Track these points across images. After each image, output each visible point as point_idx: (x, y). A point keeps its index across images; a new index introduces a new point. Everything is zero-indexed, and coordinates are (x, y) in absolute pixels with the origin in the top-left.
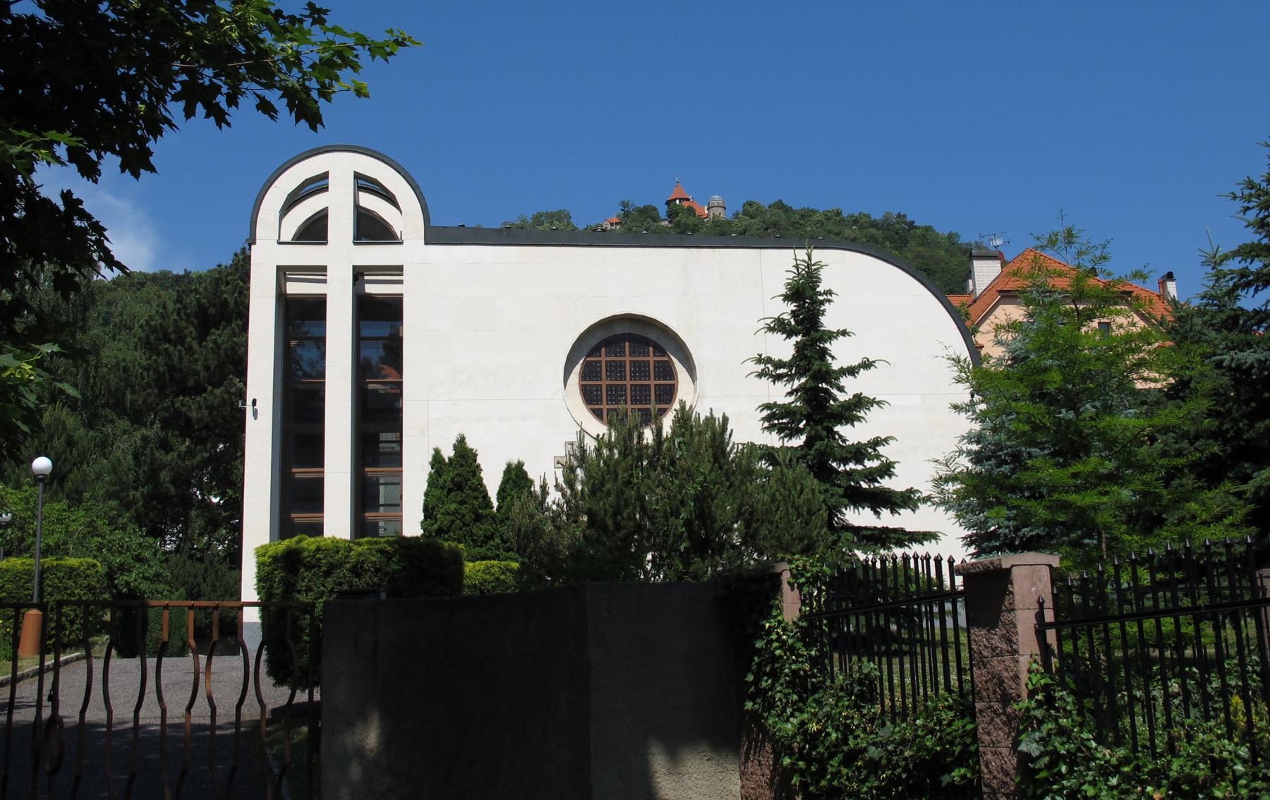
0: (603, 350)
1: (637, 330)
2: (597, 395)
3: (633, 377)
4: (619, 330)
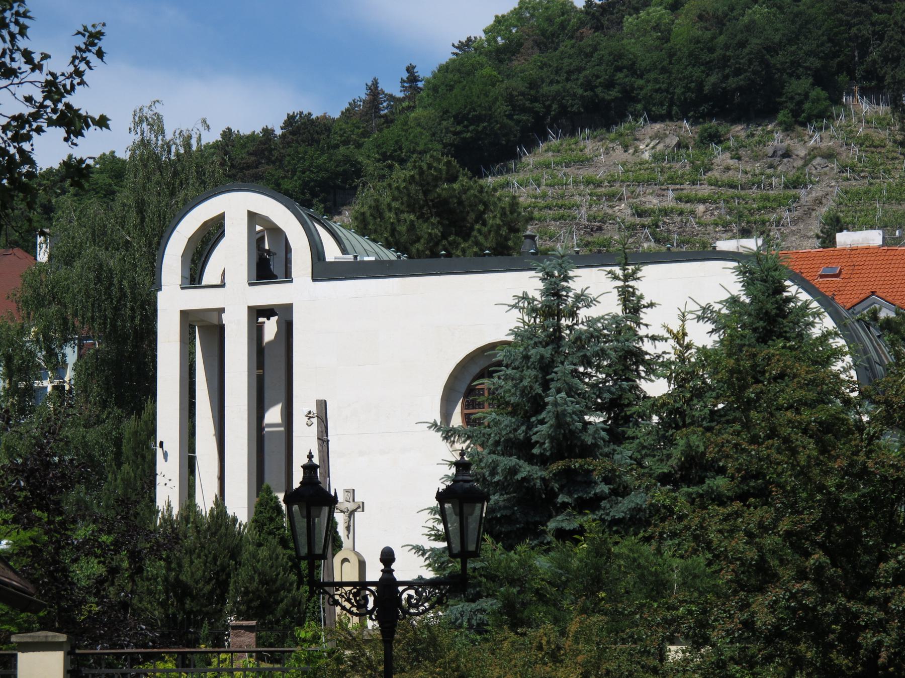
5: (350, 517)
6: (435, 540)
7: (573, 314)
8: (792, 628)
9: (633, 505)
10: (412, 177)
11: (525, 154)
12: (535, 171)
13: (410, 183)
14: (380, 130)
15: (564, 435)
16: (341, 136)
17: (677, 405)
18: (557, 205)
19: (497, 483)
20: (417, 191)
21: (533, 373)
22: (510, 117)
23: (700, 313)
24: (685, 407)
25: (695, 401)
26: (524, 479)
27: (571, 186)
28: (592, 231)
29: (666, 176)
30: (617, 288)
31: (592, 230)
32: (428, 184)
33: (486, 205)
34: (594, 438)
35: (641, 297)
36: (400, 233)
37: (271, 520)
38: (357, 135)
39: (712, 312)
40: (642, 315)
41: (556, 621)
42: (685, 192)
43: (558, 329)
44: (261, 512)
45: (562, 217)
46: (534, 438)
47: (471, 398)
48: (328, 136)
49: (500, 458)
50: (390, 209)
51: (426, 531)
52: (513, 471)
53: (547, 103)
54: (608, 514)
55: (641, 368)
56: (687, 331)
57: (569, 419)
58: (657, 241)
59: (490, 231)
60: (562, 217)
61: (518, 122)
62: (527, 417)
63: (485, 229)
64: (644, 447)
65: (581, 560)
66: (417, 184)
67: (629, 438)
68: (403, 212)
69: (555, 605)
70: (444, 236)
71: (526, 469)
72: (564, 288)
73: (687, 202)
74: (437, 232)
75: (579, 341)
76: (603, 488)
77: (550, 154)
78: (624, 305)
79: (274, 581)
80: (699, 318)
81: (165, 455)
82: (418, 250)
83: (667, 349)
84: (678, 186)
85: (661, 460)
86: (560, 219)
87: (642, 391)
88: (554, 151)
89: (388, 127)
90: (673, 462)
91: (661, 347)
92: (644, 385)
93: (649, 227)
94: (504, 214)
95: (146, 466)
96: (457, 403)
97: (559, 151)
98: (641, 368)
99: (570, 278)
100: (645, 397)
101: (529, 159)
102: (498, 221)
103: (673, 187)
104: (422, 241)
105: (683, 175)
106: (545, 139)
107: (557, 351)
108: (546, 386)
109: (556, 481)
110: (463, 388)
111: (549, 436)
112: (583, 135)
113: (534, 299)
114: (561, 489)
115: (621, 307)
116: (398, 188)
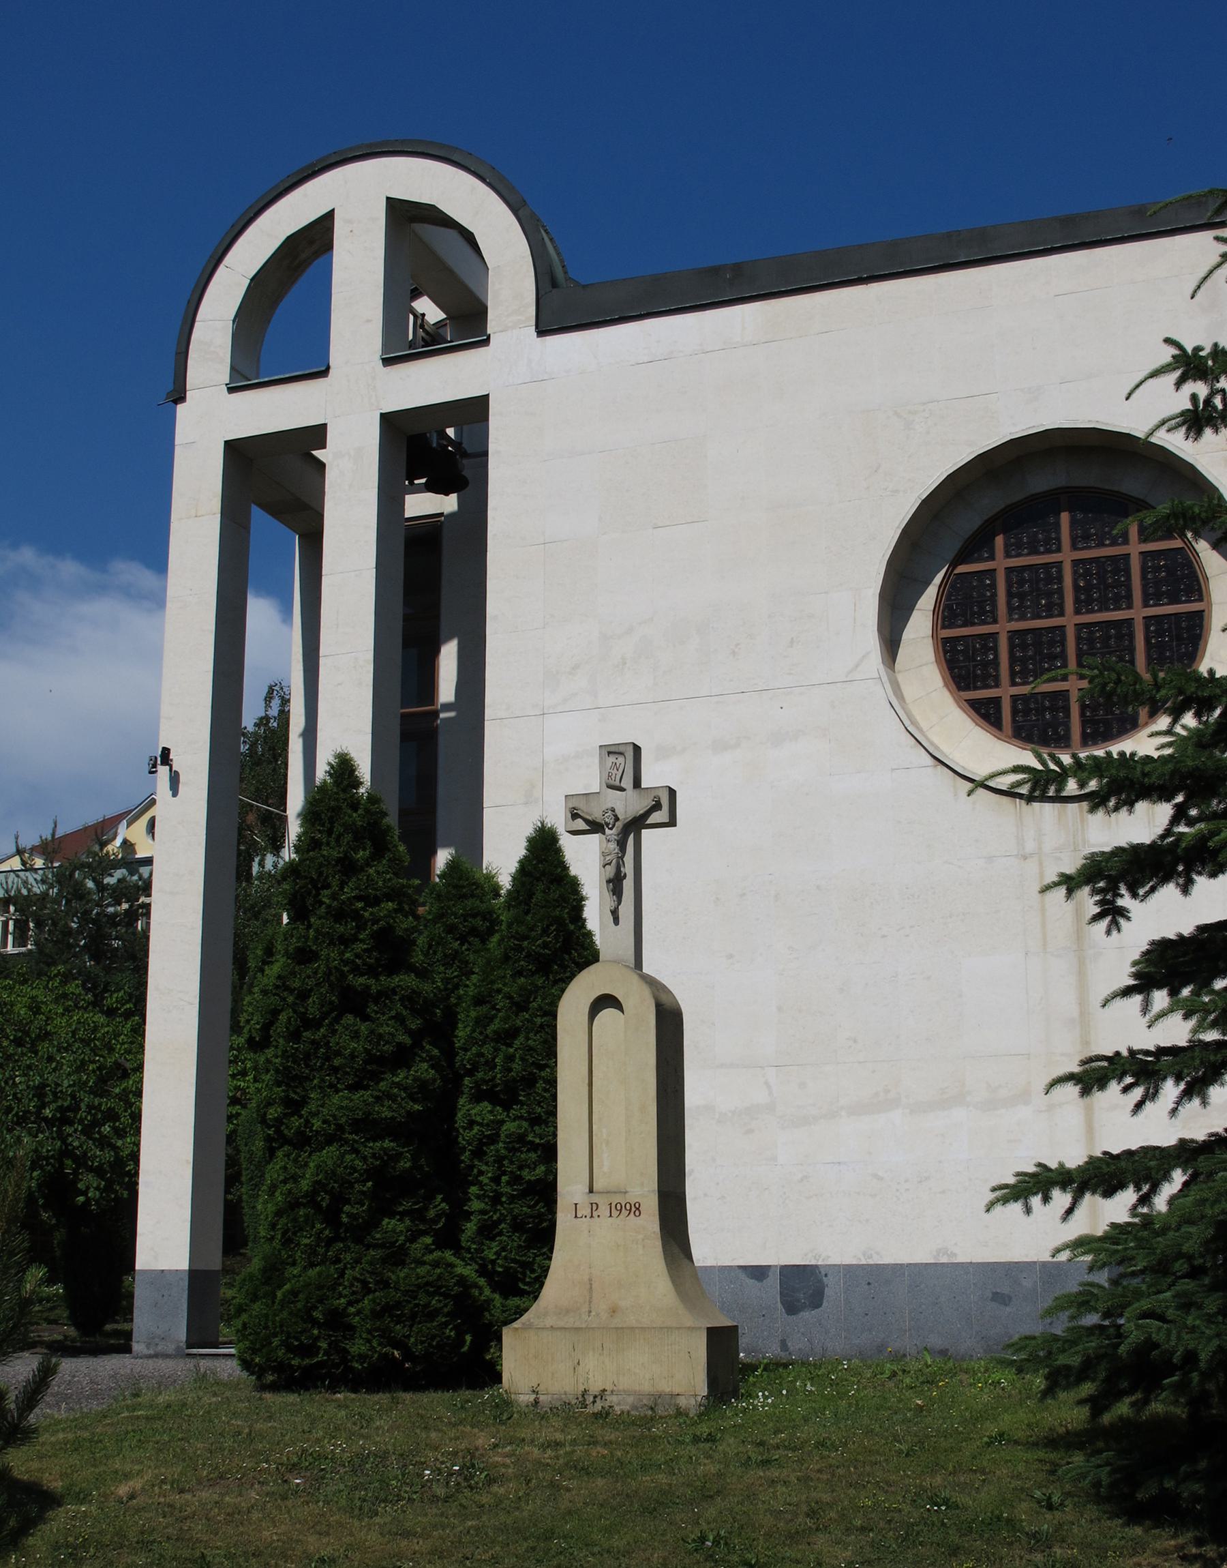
0: (999, 541)
1: (1087, 477)
2: (985, 665)
3: (1056, 608)
4: (1041, 481)
5: (622, 845)
6: (1096, 801)
81: (175, 780)
96: (927, 583)
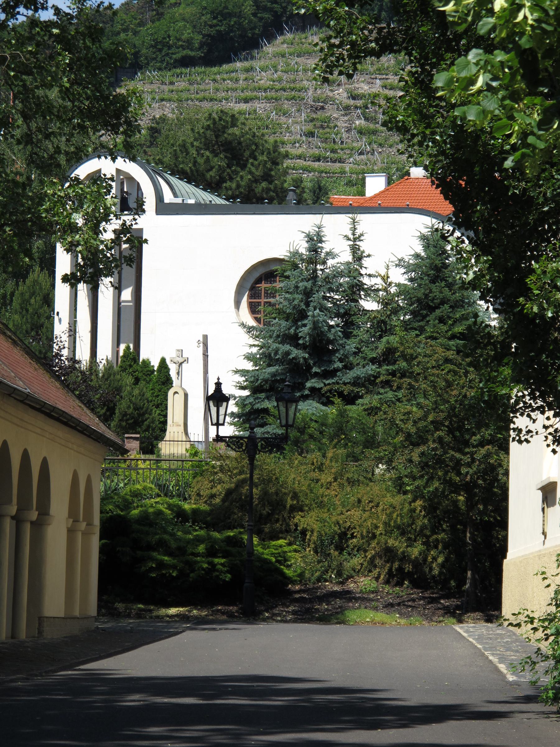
7: (324, 263)
8: (433, 463)
9: (355, 375)
10: (209, 126)
11: (265, 45)
12: (274, 59)
13: (207, 130)
14: (153, 22)
15: (317, 334)
16: (122, 25)
17: (382, 318)
18: (290, 88)
19: (278, 359)
20: (211, 135)
21: (300, 296)
22: (254, 15)
23: (397, 262)
24: (387, 319)
25: (393, 316)
26: (293, 358)
27: (301, 73)
28: (316, 110)
29: (375, 67)
30: (349, 245)
31: (316, 109)
32: (219, 130)
33: (256, 145)
34: (335, 336)
35: (363, 252)
36: (199, 164)
37: (131, 366)
38: (134, 24)
39: (404, 262)
40: (363, 262)
41: (320, 449)
42: (389, 81)
43: (315, 271)
44: (124, 361)
45: (293, 98)
46: (300, 335)
47: (254, 293)
48: (112, 26)
49: (281, 346)
50: (193, 146)
51: (235, 384)
52: (288, 353)
53: (284, 5)
54: (341, 380)
55: (362, 293)
56: (389, 275)
57: (320, 325)
58: (366, 119)
59: (259, 165)
60: (293, 98)
61: (261, 19)
62: (295, 322)
63: (256, 163)
64: (362, 341)
65: (333, 419)
66: (211, 130)
67: (354, 336)
68: (201, 149)
69: (319, 441)
70: (229, 166)
71: (295, 353)
72: (319, 247)
73: (391, 89)
74: (223, 164)
75: (327, 280)
76: (339, 365)
77: (285, 45)
78: (354, 256)
79: (142, 408)
80: (397, 265)
81: (60, 320)
82: (211, 176)
83: (378, 282)
84: (384, 76)
85: (372, 350)
86: (292, 99)
87: (362, 306)
88: (288, 44)
89: (159, 20)
90: (379, 351)
91: (374, 281)
92: (362, 302)
93: (360, 108)
94: (269, 153)
95: (29, 316)
97: (292, 44)
98: (362, 293)
99: (324, 242)
100: (364, 310)
101: (269, 49)
102: (265, 158)
103: (380, 77)
104: (214, 170)
105: (388, 68)
106: (282, 34)
107: (314, 284)
108: (307, 304)
109: (312, 359)
110: (249, 285)
111: (309, 334)
112: (312, 32)
113: (302, 254)
114: (314, 364)
115: (351, 257)
116: (198, 133)
